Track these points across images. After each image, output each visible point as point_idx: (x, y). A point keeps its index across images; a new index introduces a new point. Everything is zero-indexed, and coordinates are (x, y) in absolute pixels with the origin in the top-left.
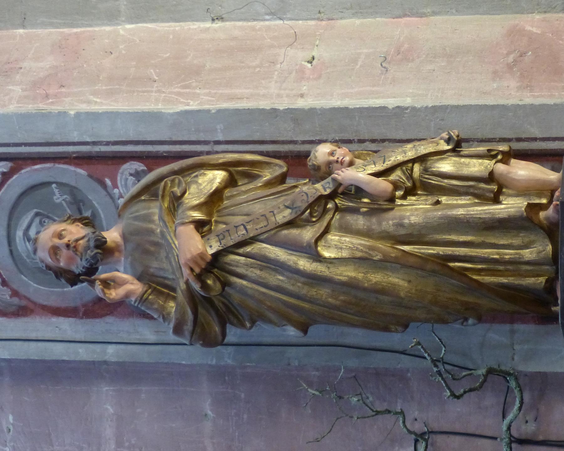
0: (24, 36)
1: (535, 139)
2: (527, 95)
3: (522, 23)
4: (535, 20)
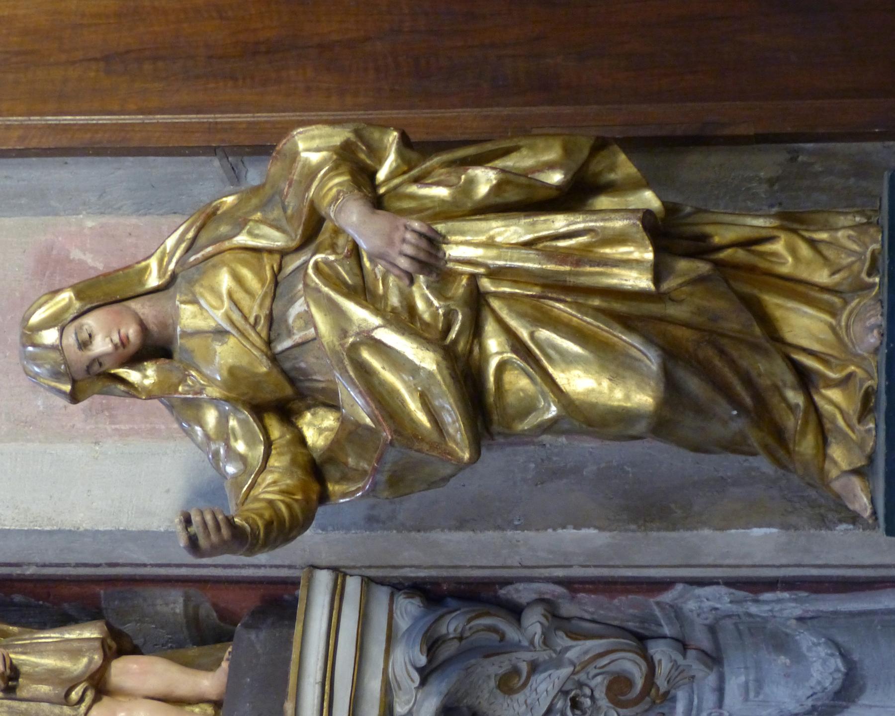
0: (631, 475)
1: (145, 565)
2: (106, 429)
3: (60, 239)
4: (86, 231)
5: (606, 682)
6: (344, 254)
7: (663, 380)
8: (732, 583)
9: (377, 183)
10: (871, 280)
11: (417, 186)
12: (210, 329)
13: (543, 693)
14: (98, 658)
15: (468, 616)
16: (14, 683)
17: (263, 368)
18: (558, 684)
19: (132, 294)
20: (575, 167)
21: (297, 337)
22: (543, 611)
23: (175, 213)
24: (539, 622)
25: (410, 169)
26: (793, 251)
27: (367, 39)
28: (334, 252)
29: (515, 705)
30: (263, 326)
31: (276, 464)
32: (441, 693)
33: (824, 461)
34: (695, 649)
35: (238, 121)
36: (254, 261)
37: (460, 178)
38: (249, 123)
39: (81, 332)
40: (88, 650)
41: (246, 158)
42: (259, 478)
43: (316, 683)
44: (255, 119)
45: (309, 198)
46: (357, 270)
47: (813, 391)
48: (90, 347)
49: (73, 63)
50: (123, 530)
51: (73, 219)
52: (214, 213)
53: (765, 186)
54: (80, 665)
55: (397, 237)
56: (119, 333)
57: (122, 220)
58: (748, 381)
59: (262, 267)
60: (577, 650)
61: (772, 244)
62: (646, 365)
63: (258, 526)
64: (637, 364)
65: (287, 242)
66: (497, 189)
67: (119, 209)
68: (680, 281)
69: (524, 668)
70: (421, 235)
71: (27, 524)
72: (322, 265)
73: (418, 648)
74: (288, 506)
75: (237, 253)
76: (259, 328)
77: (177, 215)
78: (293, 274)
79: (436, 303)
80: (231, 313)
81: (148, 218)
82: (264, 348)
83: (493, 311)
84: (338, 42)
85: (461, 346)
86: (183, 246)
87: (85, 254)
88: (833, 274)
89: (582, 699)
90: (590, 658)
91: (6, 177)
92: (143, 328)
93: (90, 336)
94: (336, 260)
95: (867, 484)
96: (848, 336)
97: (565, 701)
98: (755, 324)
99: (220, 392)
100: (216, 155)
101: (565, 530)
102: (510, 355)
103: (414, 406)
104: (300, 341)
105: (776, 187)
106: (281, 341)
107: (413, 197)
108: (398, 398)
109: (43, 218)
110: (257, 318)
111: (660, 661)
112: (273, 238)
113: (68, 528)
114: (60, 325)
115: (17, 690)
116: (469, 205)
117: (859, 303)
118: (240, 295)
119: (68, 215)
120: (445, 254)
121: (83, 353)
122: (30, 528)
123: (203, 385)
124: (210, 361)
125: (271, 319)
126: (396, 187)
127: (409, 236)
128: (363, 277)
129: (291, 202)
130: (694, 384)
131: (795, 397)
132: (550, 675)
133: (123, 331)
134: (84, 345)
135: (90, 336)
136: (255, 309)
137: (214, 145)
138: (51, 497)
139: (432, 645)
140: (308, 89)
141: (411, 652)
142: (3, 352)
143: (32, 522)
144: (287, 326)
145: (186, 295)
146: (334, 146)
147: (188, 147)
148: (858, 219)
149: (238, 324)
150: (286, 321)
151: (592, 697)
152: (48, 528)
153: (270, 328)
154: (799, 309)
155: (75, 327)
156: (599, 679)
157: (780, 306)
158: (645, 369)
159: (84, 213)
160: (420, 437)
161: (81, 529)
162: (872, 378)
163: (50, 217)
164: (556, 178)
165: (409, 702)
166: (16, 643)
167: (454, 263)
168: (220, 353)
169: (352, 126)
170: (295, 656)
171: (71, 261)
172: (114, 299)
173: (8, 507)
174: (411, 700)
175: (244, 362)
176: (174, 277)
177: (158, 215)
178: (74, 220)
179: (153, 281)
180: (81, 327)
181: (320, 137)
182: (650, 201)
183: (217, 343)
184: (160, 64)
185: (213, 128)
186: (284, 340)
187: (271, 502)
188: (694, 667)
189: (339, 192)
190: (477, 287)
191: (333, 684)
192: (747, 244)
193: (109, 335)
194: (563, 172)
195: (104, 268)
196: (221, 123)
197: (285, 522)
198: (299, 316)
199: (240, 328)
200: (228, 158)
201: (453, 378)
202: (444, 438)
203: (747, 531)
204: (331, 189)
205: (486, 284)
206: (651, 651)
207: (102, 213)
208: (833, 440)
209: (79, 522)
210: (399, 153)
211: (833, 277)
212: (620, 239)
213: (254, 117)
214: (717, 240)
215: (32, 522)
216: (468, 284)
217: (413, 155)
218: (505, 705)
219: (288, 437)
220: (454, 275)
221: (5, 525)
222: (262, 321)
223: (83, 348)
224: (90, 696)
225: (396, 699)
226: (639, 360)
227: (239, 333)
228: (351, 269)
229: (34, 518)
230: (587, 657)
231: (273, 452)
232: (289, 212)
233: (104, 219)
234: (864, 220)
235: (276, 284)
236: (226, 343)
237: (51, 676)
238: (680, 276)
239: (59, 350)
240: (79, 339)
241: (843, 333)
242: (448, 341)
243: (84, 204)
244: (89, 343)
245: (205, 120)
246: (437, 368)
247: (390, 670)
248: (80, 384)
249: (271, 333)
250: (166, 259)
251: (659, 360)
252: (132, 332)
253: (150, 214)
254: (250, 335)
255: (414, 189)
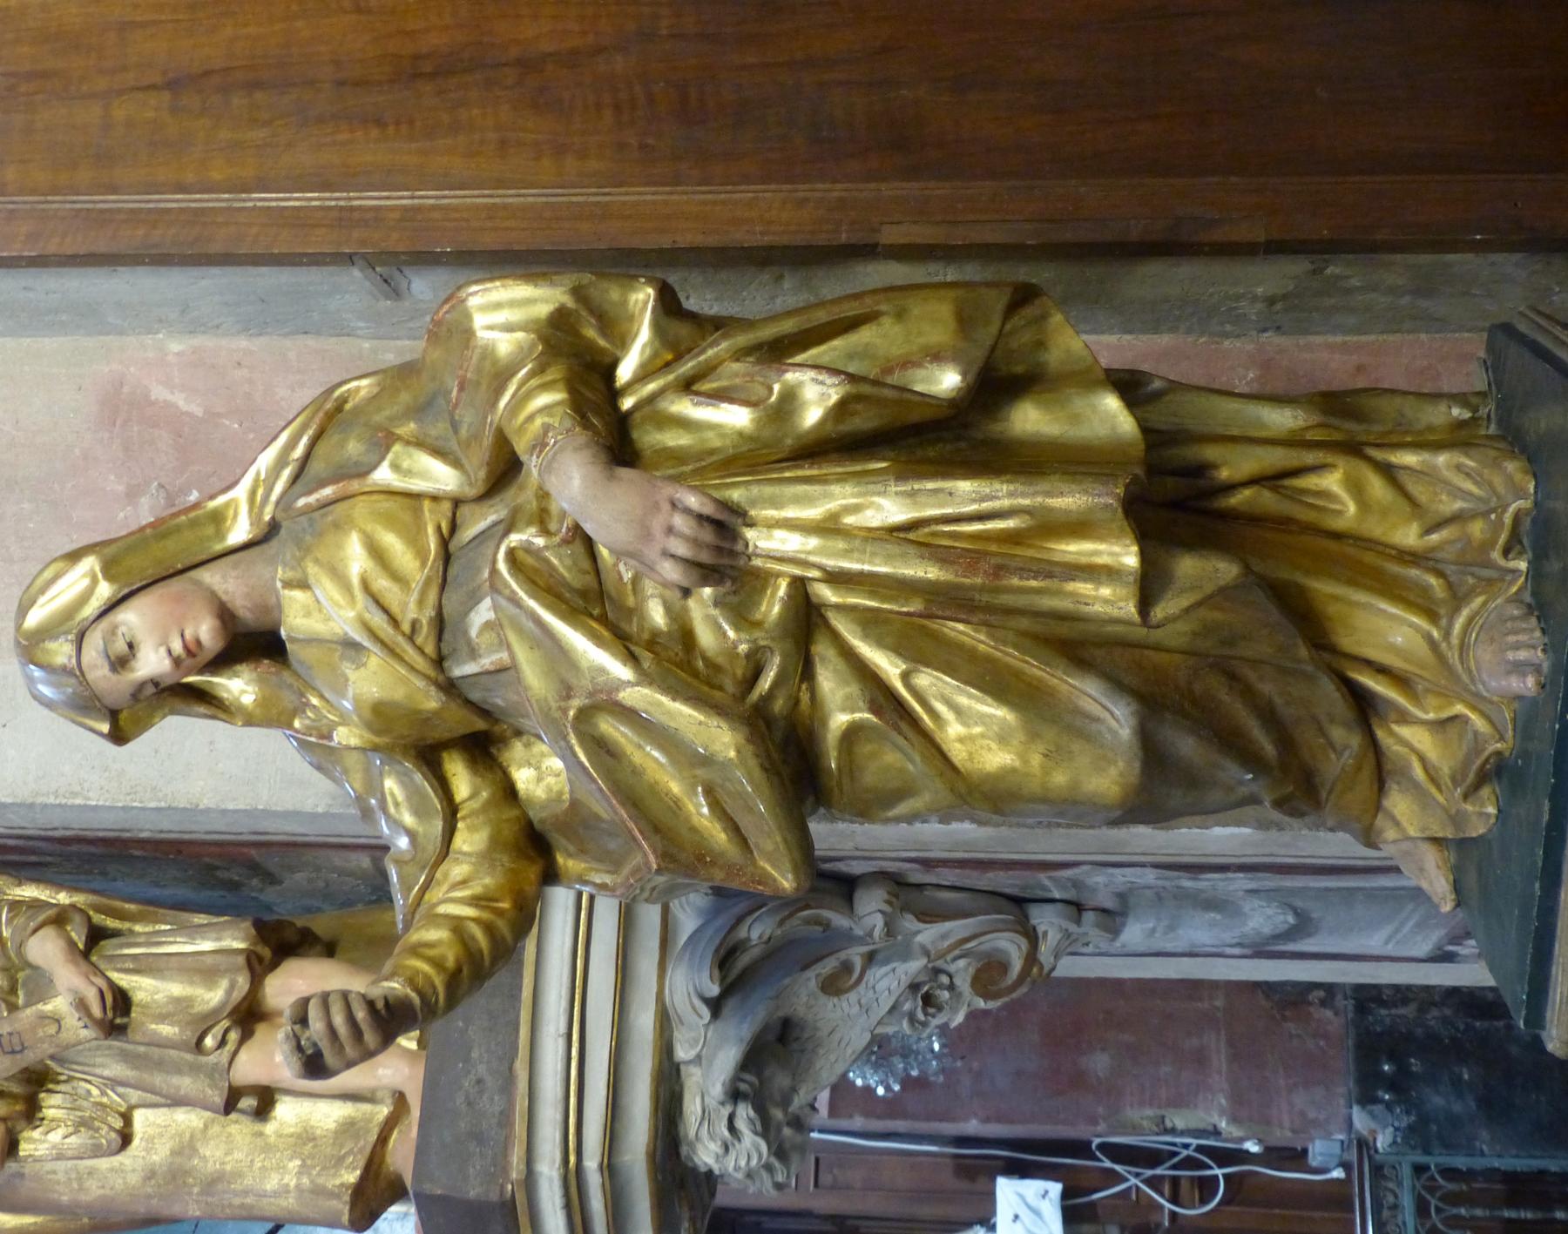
3: (132, 369)
4: (170, 358)
5: (971, 971)
6: (561, 535)
7: (1140, 754)
8: (1157, 866)
9: (618, 384)
10: (1512, 564)
11: (692, 400)
12: (335, 639)
13: (883, 992)
14: (243, 982)
15: (778, 918)
16: (125, 1020)
17: (432, 701)
18: (905, 981)
19: (204, 557)
20: (979, 354)
21: (487, 662)
22: (886, 896)
23: (306, 333)
24: (880, 911)
25: (679, 357)
26: (1356, 488)
27: (599, 50)
28: (545, 531)
29: (845, 1004)
30: (427, 638)
31: (466, 848)
32: (742, 1040)
33: (1375, 816)
34: (1093, 910)
35: (387, 206)
36: (407, 517)
37: (771, 390)
38: (405, 209)
39: (114, 641)
40: (227, 971)
41: (407, 271)
42: (439, 871)
43: (559, 1036)
44: (416, 201)
45: (495, 425)
46: (586, 564)
47: (1375, 722)
48: (133, 663)
49: (120, 92)
50: (263, 810)
51: (148, 340)
52: (339, 408)
53: (1259, 306)
54: (213, 996)
55: (657, 525)
56: (182, 636)
57: (224, 342)
58: (1270, 717)
59: (420, 528)
60: (928, 934)
61: (1320, 476)
62: (1110, 730)
63: (434, 988)
64: (1094, 727)
65: (461, 485)
66: (841, 410)
67: (218, 327)
68: (1185, 601)
69: (858, 963)
70: (701, 518)
71: (122, 797)
72: (521, 555)
73: (706, 974)
74: (489, 928)
75: (376, 501)
76: (419, 640)
77: (309, 335)
78: (477, 541)
79: (731, 634)
80: (367, 616)
81: (263, 340)
82: (432, 673)
83: (836, 637)
84: (550, 54)
85: (779, 705)
86: (286, 473)
87: (173, 393)
88: (1428, 531)
89: (938, 992)
90: (951, 945)
91: (25, 288)
92: (225, 615)
93: (131, 646)
94: (546, 547)
95: (1446, 853)
96: (1462, 663)
97: (915, 1000)
98: (1300, 642)
99: (361, 737)
100: (353, 264)
101: (926, 825)
102: (867, 715)
103: (700, 811)
104: (492, 668)
105: (1279, 306)
106: (460, 663)
107: (684, 423)
108: (667, 795)
109: (102, 338)
110: (415, 625)
111: (1045, 933)
112: (440, 476)
113: (182, 806)
114: (74, 631)
115: (129, 1031)
116: (789, 442)
117: (1485, 604)
118: (382, 583)
119: (139, 334)
120: (747, 545)
121: (119, 677)
122: (126, 804)
123: (333, 721)
124: (341, 686)
125: (440, 623)
126: (652, 399)
127: (679, 521)
128: (597, 572)
129: (467, 417)
130: (1186, 746)
131: (1347, 738)
132: (894, 970)
133: (188, 634)
134: (120, 663)
135: (131, 646)
136: (412, 608)
137: (347, 251)
138: (156, 752)
139: (725, 959)
140: (503, 143)
141: (696, 977)
142: (67, 535)
143: (129, 794)
144: (469, 642)
145: (293, 568)
146: (536, 321)
147: (306, 254)
148: (1456, 412)
149: (382, 635)
150: (466, 633)
151: (951, 987)
152: (153, 805)
153: (440, 638)
154: (1372, 605)
155: (102, 631)
156: (962, 963)
157: (1336, 598)
158: (1108, 736)
159: (164, 331)
160: (708, 859)
161: (201, 807)
162: (1502, 738)
163: (111, 337)
164: (947, 381)
165: (696, 1041)
166: (126, 951)
167: (763, 559)
168: (354, 683)
169: (570, 279)
170: (526, 993)
171: (153, 404)
172: (171, 571)
173: (93, 768)
174: (699, 1040)
175: (399, 694)
176: (273, 529)
177: (279, 335)
178: (150, 342)
179: (239, 532)
180: (113, 631)
181: (512, 304)
182: (1114, 417)
183: (348, 665)
184: (259, 96)
185: (346, 218)
186: (464, 663)
187: (457, 925)
188: (1091, 933)
189: (546, 428)
190: (807, 596)
191: (583, 1089)
192: (1273, 479)
193: (164, 642)
194: (958, 368)
195: (204, 413)
196: (360, 208)
197: (482, 955)
198: (488, 626)
199: (386, 640)
200: (374, 269)
201: (766, 770)
202: (751, 852)
203: (1204, 831)
204: (531, 418)
205: (827, 594)
206: (1034, 922)
207: (191, 332)
208: (1395, 787)
209: (198, 795)
210: (657, 327)
211: (1426, 538)
212: (1078, 527)
213: (413, 197)
214: (1224, 474)
215: (129, 794)
216: (789, 595)
217: (683, 330)
218: (830, 1005)
219: (485, 794)
220: (761, 580)
221: (89, 799)
222: (425, 629)
223: (119, 669)
224: (233, 1036)
225: (676, 1034)
226: (1098, 720)
227: (385, 651)
228: (575, 563)
229: (132, 788)
230: (946, 944)
231: (460, 825)
232: (464, 432)
233: (198, 341)
234: (1467, 415)
235: (447, 557)
236: (364, 665)
237: (178, 1009)
238: (1183, 591)
239: (75, 675)
240: (110, 653)
241: (1453, 657)
242: (755, 695)
243: (160, 321)
244: (131, 657)
245: (333, 203)
246: (737, 756)
247: (667, 991)
248: (123, 716)
249: (442, 645)
250: (260, 492)
251: (1133, 721)
252: (206, 631)
253: (267, 333)
254: (404, 651)
255: (685, 407)
